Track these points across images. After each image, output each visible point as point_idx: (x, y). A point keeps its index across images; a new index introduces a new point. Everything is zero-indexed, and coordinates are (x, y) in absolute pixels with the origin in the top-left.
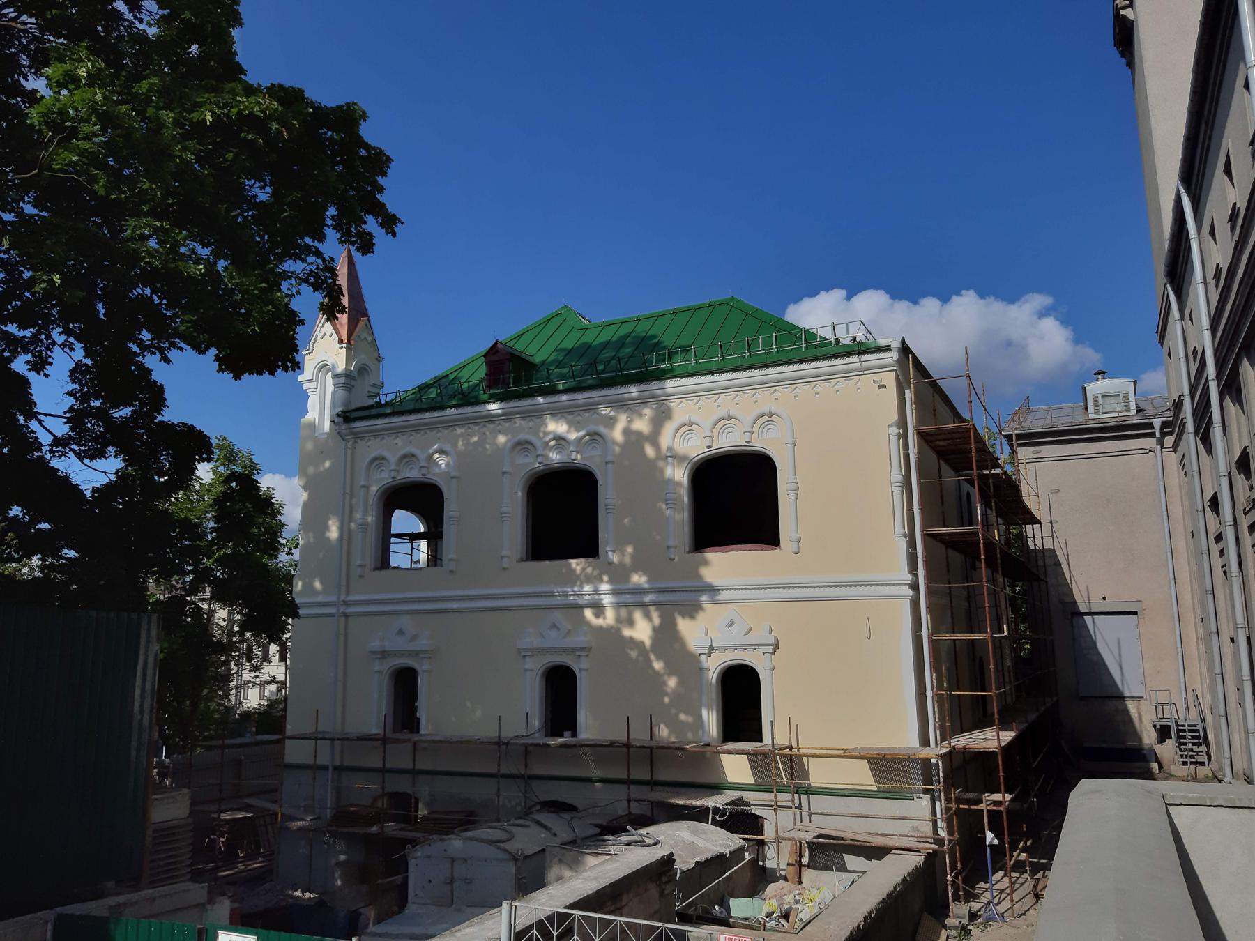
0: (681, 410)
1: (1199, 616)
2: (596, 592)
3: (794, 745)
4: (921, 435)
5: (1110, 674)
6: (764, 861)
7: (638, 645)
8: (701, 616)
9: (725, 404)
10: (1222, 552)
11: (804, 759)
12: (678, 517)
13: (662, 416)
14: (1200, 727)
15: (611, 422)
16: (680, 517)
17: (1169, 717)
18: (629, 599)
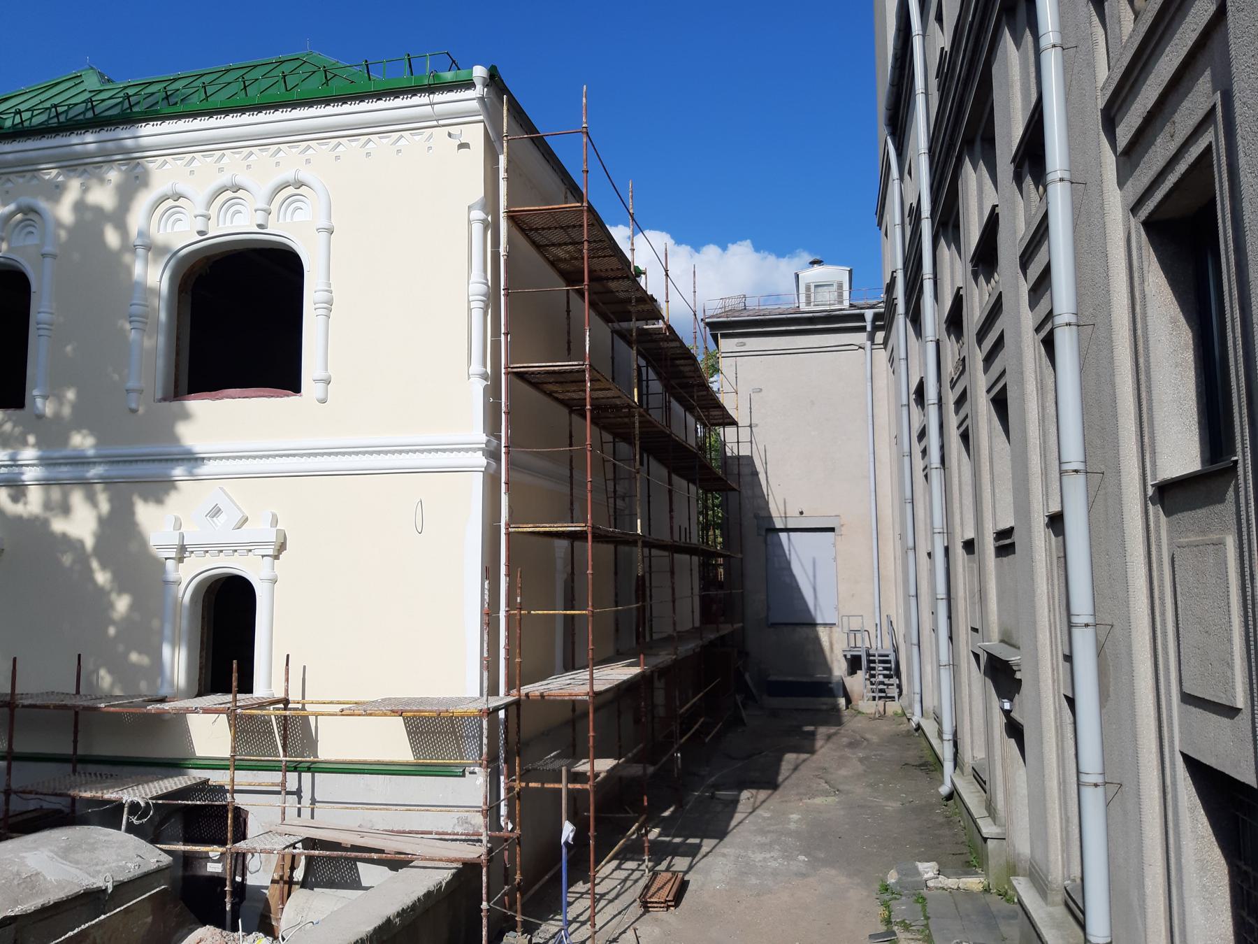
0: (165, 175)
1: (898, 531)
2: (14, 462)
3: (295, 695)
4: (512, 218)
6: (243, 876)
7: (74, 545)
8: (173, 499)
9: (232, 166)
10: (924, 452)
12: (148, 343)
13: (136, 180)
14: (892, 658)
15: (56, 191)
16: (151, 345)
17: (863, 644)
18: (66, 473)
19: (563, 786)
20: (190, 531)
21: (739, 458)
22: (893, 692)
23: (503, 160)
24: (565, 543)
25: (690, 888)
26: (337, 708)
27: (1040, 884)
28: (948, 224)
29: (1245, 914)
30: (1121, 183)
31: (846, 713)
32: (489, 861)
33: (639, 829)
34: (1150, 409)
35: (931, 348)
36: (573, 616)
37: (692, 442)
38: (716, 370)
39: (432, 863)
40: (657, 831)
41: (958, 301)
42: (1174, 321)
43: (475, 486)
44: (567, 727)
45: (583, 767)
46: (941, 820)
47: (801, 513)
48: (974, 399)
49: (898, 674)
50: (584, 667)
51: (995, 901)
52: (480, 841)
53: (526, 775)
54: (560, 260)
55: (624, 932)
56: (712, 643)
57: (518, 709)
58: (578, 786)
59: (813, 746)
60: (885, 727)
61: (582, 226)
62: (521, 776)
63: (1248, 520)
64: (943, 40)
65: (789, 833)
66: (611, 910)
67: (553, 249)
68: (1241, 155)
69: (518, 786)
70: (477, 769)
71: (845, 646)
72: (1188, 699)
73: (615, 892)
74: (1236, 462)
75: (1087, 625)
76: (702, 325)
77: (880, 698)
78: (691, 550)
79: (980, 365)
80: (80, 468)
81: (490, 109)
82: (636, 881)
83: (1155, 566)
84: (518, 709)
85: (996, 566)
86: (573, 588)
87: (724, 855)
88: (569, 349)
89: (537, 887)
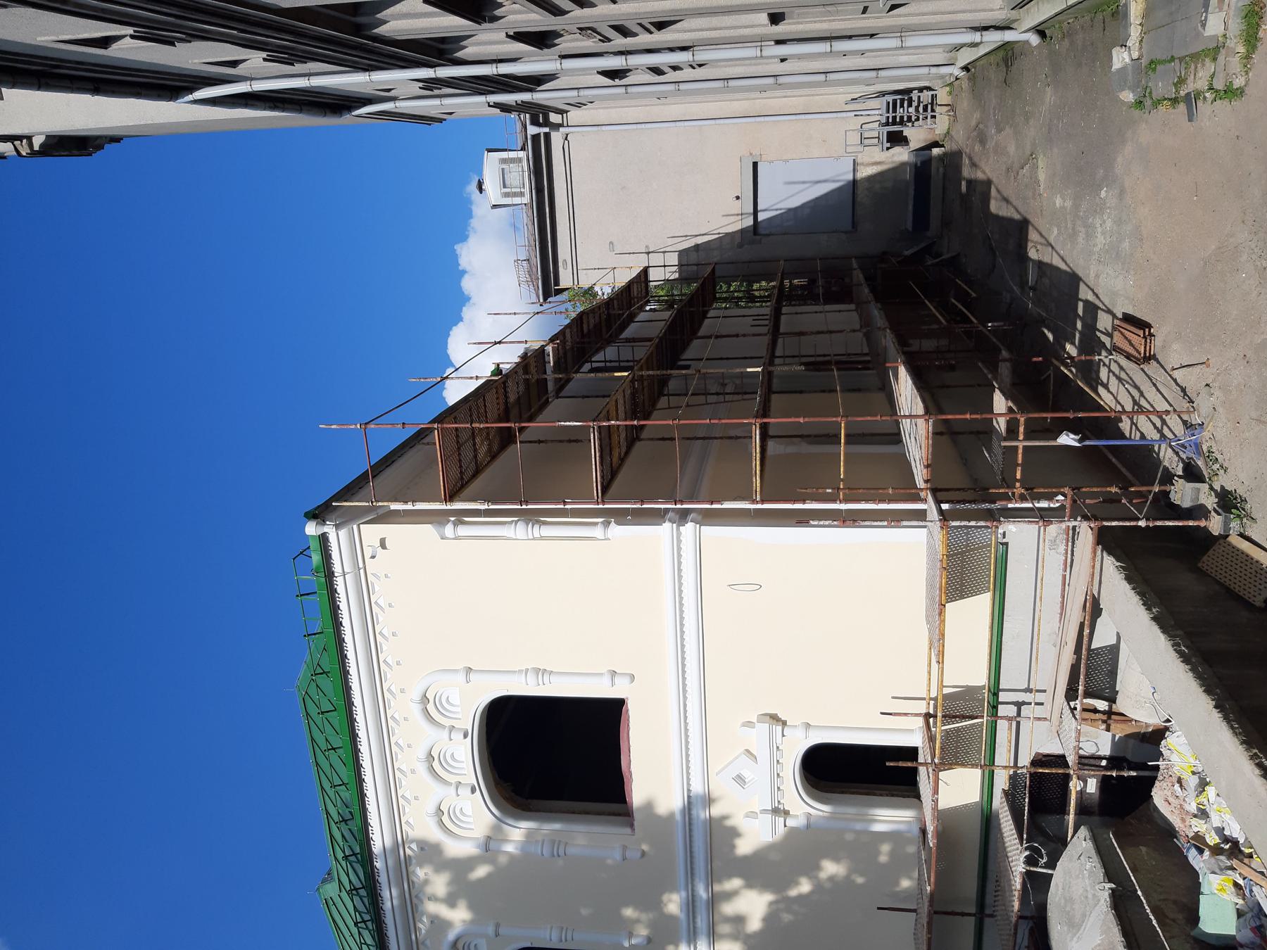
1: (757, 94)
3: (922, 707)
4: (451, 497)
6: (1101, 758)
9: (409, 761)
10: (675, 68)
11: (946, 691)
13: (430, 852)
14: (890, 98)
15: (439, 924)
16: (583, 838)
17: (876, 130)
20: (762, 802)
80: (698, 904)
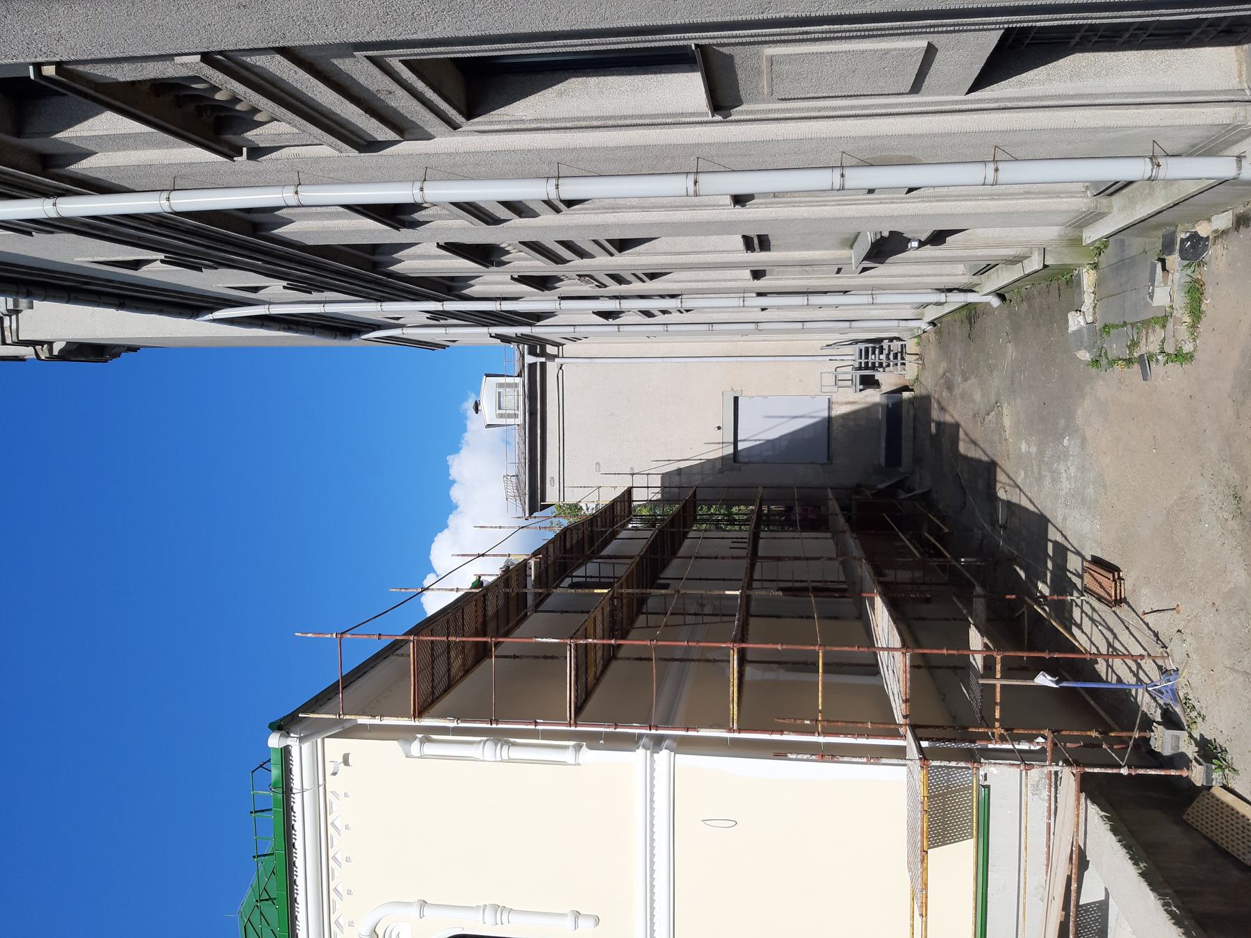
1: (738, 337)
4: (420, 713)
5: (802, 429)
10: (664, 312)
17: (848, 373)
19: (998, 683)
21: (663, 487)
22: (896, 346)
23: (363, 720)
24: (749, 669)
25: (1099, 555)
26: (918, 919)
27: (1092, 217)
28: (449, 287)
29: (1120, 41)
30: (429, 137)
31: (918, 391)
32: (1078, 765)
33: (1040, 605)
34: (641, 117)
35: (567, 304)
36: (824, 664)
37: (648, 534)
38: (575, 507)
39: (1081, 826)
40: (1040, 585)
41: (523, 280)
42: (560, 94)
43: (689, 762)
44: (936, 675)
45: (978, 661)
46: (1025, 306)
47: (719, 428)
48: (622, 275)
49: (879, 341)
50: (875, 655)
51: (1104, 260)
52: (1056, 773)
53: (988, 722)
54: (464, 664)
55: (1147, 625)
56: (848, 520)
57: (920, 727)
58: (998, 667)
59: (951, 425)
60: (932, 354)
61: (432, 642)
62: (988, 727)
63: (752, 36)
64: (275, 287)
65: (1041, 453)
66: (1124, 636)
67: (453, 671)
68: (415, 37)
69: (999, 731)
70: (982, 772)
71: (851, 390)
72: (916, 88)
73: (1105, 631)
74: (697, 46)
75: (842, 176)
76: (531, 521)
77: (903, 358)
78: (755, 538)
79: (586, 261)
81: (313, 731)
82: (1093, 609)
83: (788, 115)
84: (920, 727)
85: (779, 250)
86: (794, 663)
87: (1065, 519)
88: (552, 657)
89: (1102, 713)
